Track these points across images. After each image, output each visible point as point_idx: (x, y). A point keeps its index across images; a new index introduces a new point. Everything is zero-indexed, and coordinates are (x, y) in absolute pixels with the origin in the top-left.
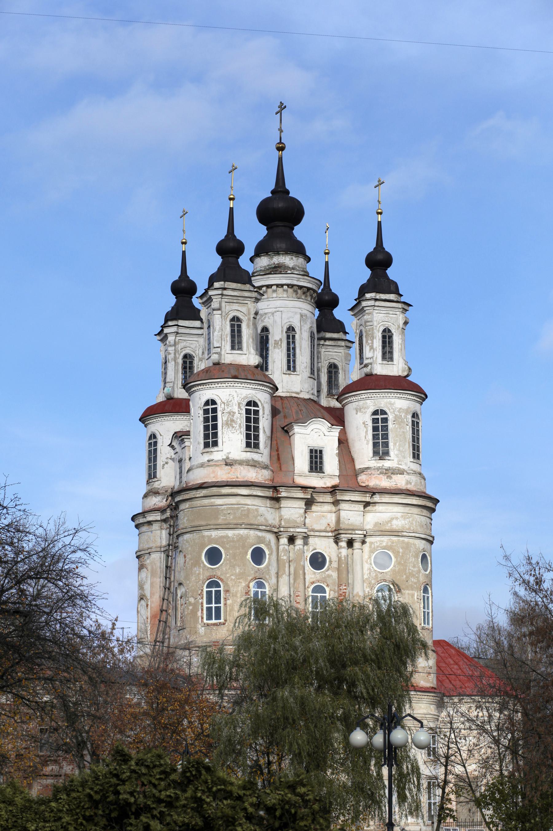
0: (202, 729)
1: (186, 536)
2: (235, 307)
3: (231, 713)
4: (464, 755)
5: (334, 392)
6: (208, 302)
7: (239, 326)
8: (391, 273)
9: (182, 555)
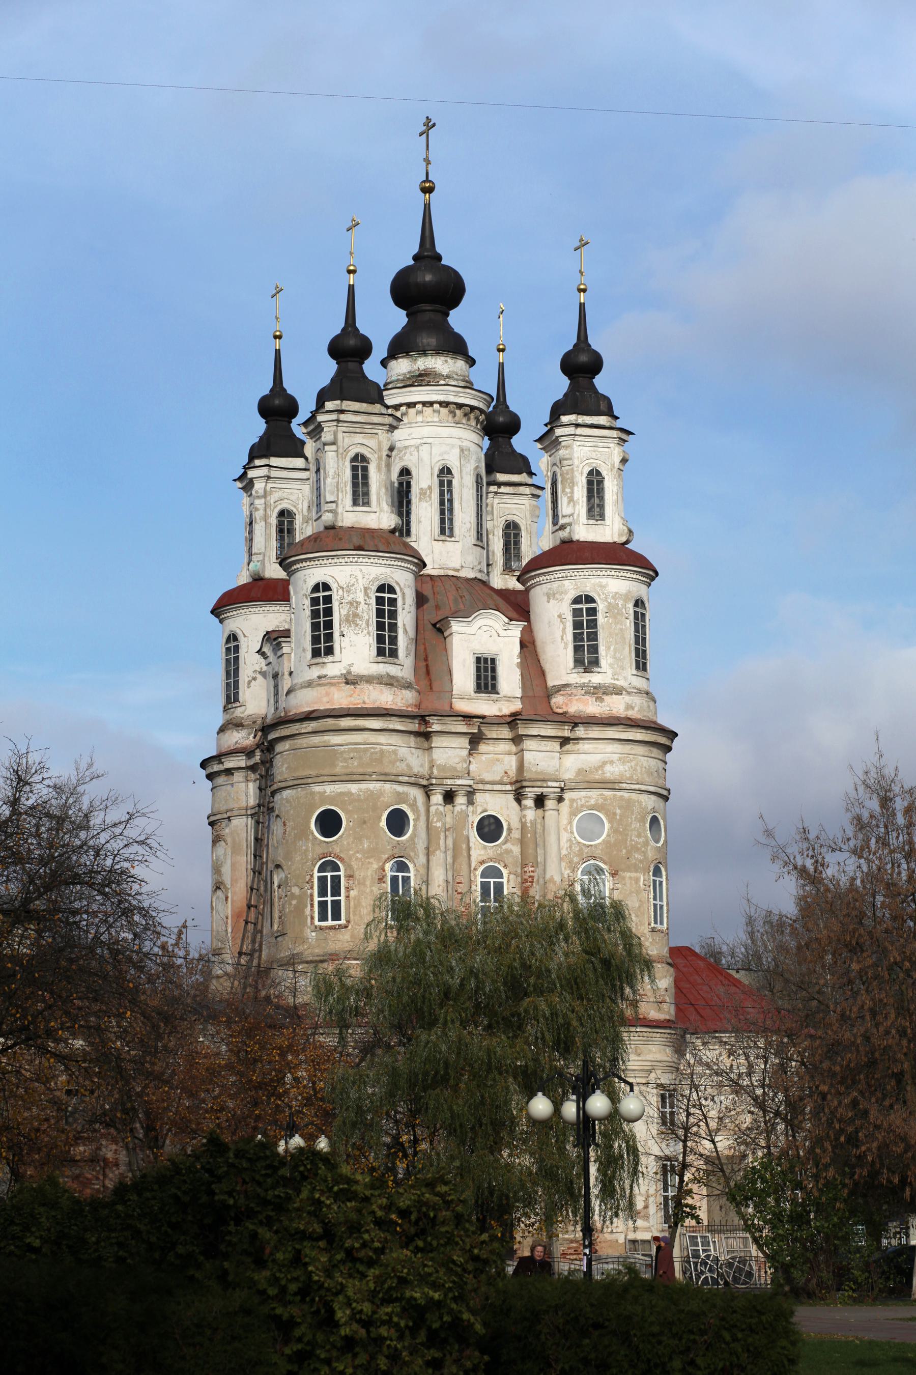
0: (314, 1089)
1: (286, 794)
2: (359, 439)
3: (358, 1065)
4: (713, 1125)
5: (514, 565)
6: (316, 431)
7: (365, 469)
8: (601, 382)
9: (279, 822)
